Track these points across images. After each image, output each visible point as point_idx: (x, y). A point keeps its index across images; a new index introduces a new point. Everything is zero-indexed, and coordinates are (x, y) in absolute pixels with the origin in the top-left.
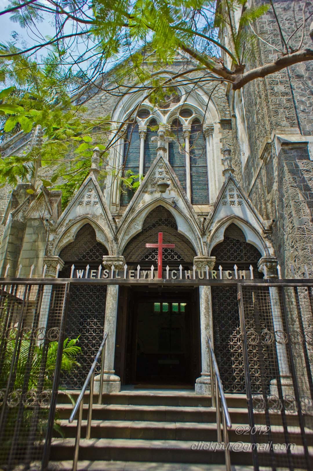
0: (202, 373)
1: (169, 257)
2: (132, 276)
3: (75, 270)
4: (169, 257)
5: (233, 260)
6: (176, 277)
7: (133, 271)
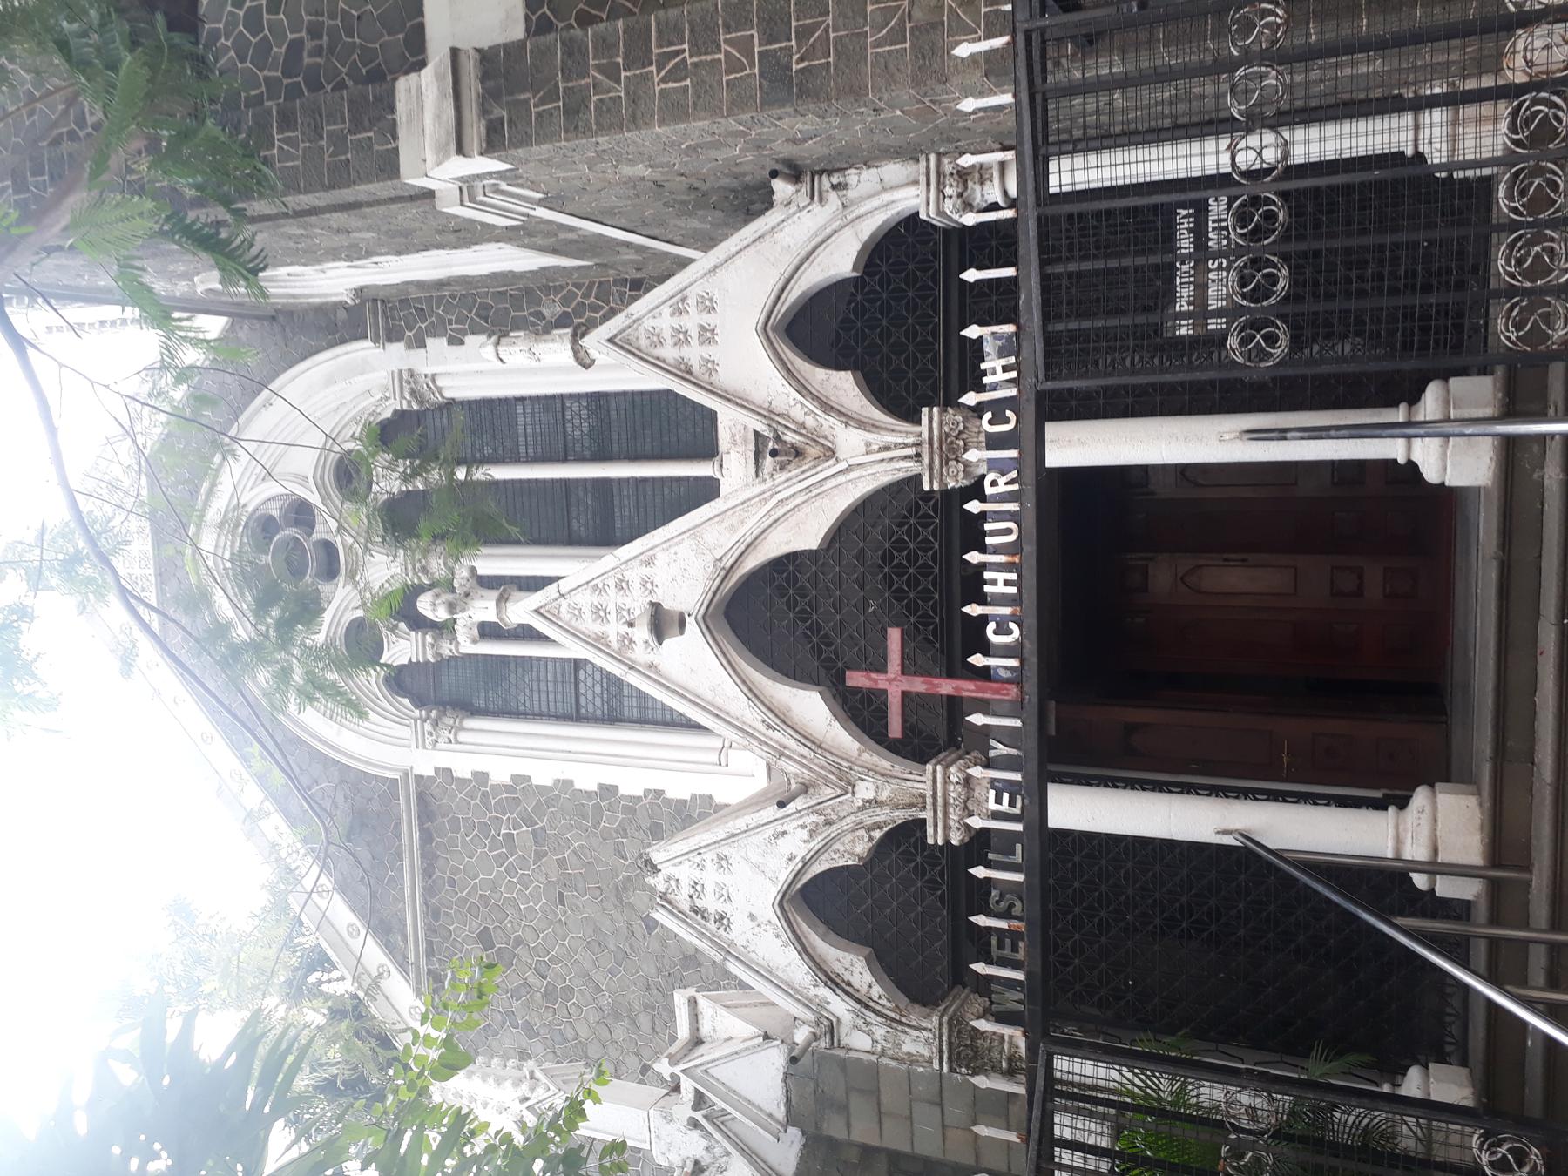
0: (1402, 460)
1: (925, 534)
2: (1015, 949)
4: (925, 534)
5: (936, 301)
6: (1012, 626)
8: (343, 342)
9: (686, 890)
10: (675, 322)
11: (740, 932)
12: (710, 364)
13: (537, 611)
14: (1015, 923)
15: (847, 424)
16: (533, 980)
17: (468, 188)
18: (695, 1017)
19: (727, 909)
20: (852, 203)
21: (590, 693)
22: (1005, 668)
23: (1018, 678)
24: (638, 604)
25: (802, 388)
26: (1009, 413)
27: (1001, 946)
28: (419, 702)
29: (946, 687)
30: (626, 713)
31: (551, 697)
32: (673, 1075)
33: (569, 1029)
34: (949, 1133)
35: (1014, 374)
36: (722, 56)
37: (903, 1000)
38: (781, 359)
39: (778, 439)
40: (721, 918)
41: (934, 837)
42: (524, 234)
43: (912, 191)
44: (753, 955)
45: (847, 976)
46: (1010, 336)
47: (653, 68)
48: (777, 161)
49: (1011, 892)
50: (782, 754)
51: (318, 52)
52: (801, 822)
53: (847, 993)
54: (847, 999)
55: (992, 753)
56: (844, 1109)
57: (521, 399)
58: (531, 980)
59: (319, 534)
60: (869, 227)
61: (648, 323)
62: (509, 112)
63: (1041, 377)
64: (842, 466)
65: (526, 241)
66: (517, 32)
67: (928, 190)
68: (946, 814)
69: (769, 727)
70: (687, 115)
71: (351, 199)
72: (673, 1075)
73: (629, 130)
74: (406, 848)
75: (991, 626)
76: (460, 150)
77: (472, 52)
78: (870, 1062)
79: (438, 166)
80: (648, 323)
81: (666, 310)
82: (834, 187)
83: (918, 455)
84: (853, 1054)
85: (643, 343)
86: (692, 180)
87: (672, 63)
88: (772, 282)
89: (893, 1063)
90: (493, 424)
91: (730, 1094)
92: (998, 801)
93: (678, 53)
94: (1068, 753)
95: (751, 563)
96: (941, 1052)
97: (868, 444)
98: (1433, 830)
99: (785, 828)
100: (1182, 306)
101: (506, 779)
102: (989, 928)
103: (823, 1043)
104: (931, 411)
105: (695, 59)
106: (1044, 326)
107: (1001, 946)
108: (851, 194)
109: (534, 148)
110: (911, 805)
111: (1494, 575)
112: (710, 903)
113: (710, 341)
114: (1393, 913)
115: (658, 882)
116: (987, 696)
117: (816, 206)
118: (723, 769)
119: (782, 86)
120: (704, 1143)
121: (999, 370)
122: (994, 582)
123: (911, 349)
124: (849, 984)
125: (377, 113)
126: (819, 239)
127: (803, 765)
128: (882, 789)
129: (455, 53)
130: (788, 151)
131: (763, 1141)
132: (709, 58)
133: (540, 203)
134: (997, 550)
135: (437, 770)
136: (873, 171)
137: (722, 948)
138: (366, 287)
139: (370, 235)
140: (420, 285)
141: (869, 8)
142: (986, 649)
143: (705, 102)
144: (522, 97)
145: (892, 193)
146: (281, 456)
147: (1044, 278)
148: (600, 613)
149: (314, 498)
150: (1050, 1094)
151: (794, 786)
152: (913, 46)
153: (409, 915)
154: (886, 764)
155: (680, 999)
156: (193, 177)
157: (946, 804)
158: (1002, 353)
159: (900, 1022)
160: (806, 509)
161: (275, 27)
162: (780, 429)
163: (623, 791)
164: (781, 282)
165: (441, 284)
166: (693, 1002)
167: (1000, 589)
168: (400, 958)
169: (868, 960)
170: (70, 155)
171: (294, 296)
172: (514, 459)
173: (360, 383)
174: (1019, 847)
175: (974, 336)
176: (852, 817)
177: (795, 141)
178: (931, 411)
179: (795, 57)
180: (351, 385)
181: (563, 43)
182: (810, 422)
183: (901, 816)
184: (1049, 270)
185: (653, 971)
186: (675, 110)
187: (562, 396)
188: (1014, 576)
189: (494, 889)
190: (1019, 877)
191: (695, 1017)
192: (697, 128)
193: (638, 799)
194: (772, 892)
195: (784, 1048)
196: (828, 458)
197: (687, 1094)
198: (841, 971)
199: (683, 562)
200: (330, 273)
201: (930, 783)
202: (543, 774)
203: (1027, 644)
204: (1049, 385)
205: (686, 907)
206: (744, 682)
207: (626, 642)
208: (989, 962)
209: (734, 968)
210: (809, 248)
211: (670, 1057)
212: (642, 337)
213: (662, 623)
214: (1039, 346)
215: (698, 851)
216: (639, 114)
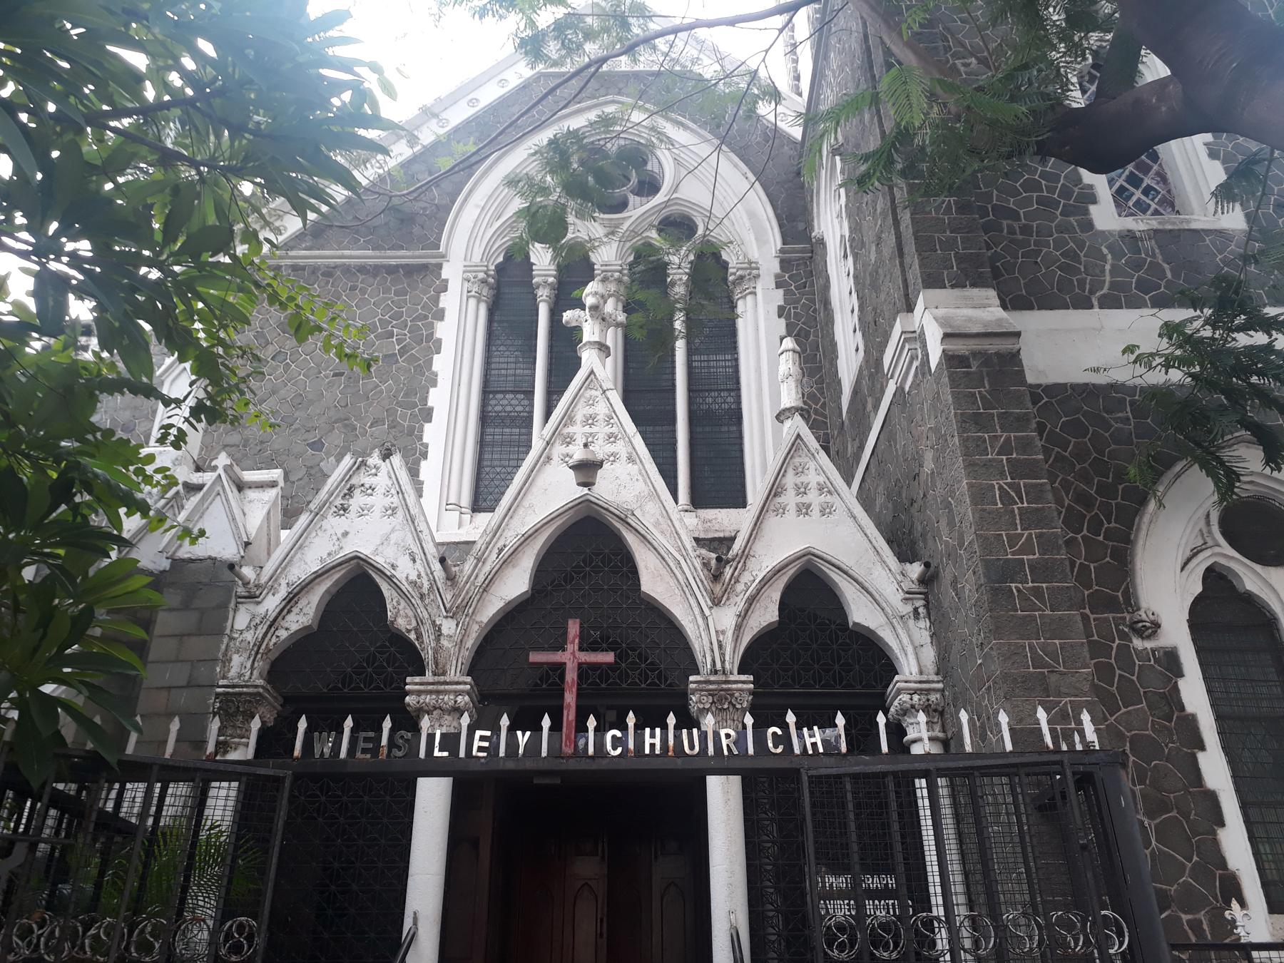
2: (364, 751)
3: (308, 732)
6: (619, 750)
7: (488, 733)
8: (781, 226)
9: (368, 481)
10: (813, 485)
11: (334, 524)
12: (782, 511)
13: (592, 372)
14: (386, 751)
16: (271, 350)
17: (918, 338)
18: (261, 486)
21: (505, 402)
22: (587, 744)
23: (581, 754)
24: (600, 450)
25: (766, 582)
27: (366, 740)
28: (500, 269)
29: (570, 698)
30: (489, 430)
31: (503, 372)
34: (164, 693)
37: (273, 656)
38: (787, 565)
39: (728, 562)
40: (344, 509)
41: (412, 683)
42: (872, 370)
43: (915, 670)
45: (295, 610)
46: (839, 749)
48: (937, 567)
49: (410, 749)
50: (479, 560)
51: (1012, 231)
52: (423, 574)
53: (282, 610)
55: (519, 733)
56: (186, 606)
58: (270, 348)
59: (633, 199)
60: (886, 635)
61: (812, 465)
63: (811, 773)
65: (866, 373)
66: (1031, 379)
68: (431, 692)
69: (501, 551)
70: (976, 505)
71: (906, 250)
74: (383, 253)
75: (619, 734)
76: (946, 336)
77: (1017, 347)
78: (225, 628)
79: (931, 320)
80: (812, 465)
81: (822, 479)
82: (916, 610)
83: (716, 672)
84: (231, 614)
85: (797, 460)
86: (920, 502)
88: (844, 560)
89: (223, 647)
90: (717, 337)
92: (482, 738)
93: (1021, 498)
94: (470, 791)
95: (630, 538)
96: (234, 686)
97: (723, 632)
99: (418, 561)
101: (438, 334)
103: (241, 590)
106: (849, 775)
107: (366, 740)
108: (911, 622)
110: (437, 664)
112: (358, 500)
113: (799, 511)
115: (374, 459)
116: (564, 730)
117: (901, 595)
119: (999, 576)
121: (813, 740)
122: (653, 736)
123: (796, 667)
124: (289, 611)
125: (970, 274)
126: (877, 597)
127: (469, 577)
128: (450, 640)
129: (1017, 335)
130: (947, 574)
133: (900, 389)
134: (678, 738)
135: (447, 281)
137: (321, 509)
138: (825, 247)
139: (873, 257)
140: (827, 286)
141: (1057, 642)
142: (601, 730)
143: (983, 519)
145: (913, 655)
146: (705, 185)
147: (884, 775)
149: (660, 198)
150: (202, 777)
153: (327, 253)
154: (470, 643)
155: (276, 474)
156: (932, 144)
157: (438, 692)
159: (257, 653)
160: (672, 582)
161: (1028, 201)
162: (735, 564)
163: (427, 426)
165: (826, 303)
166: (273, 484)
167: (648, 741)
168: (292, 244)
169: (305, 628)
170: (936, 48)
171: (818, 192)
172: (690, 352)
173: (750, 238)
174: (445, 754)
175: (837, 721)
176: (426, 616)
177: (955, 582)
180: (752, 236)
182: (740, 587)
183: (428, 656)
184: (890, 778)
185: (276, 447)
186: (980, 496)
187: (739, 389)
188: (657, 752)
190: (422, 754)
191: (261, 486)
192: (966, 511)
194: (366, 551)
195: (237, 559)
197: (196, 478)
198: (300, 605)
199: (632, 485)
200: (836, 221)
201: (456, 679)
202: (442, 364)
203: (605, 762)
204: (805, 778)
205: (353, 481)
208: (353, 730)
209: (304, 519)
211: (231, 466)
213: (587, 470)
214: (834, 771)
215: (400, 492)
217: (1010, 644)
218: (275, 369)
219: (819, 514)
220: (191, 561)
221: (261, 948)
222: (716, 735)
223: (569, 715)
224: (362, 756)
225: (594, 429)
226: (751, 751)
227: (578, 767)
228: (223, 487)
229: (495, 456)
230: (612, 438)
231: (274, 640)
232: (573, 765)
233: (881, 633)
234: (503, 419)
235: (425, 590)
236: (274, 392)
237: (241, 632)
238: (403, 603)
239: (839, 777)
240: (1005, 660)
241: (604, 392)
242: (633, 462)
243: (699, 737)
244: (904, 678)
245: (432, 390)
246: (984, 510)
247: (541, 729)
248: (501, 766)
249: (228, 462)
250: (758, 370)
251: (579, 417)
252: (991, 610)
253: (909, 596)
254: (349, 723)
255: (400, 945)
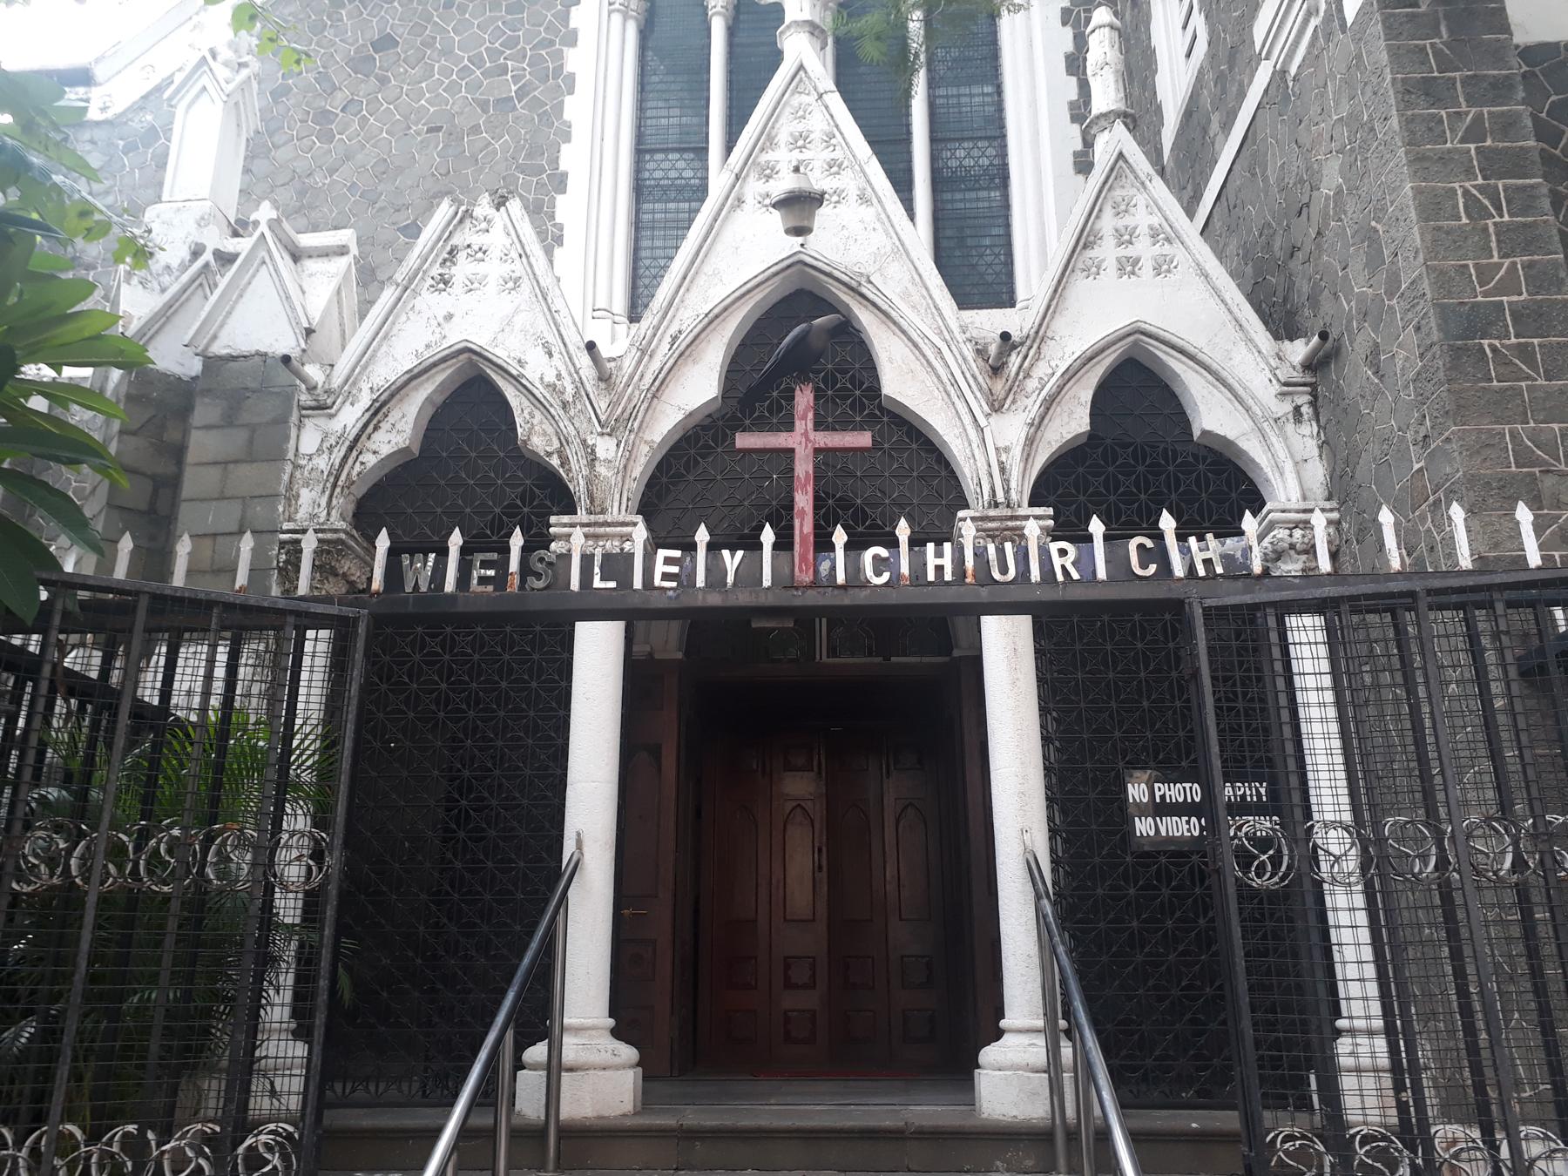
0: (1003, 1023)
3: (393, 553)
6: (886, 576)
7: (677, 553)
9: (478, 241)
10: (1143, 229)
11: (430, 302)
12: (1095, 270)
13: (801, 67)
14: (517, 580)
15: (1032, 425)
16: (340, 97)
18: (325, 253)
19: (458, 286)
20: (1281, 429)
22: (833, 568)
24: (818, 181)
25: (1071, 375)
26: (1153, 568)
29: (803, 500)
30: (646, 206)
32: (256, 223)
33: (284, 138)
35: (1201, 572)
36: (1496, 259)
37: (360, 490)
38: (1102, 350)
40: (445, 281)
43: (1295, 494)
44: (404, 318)
45: (385, 426)
46: (1249, 568)
47: (1480, 181)
49: (555, 576)
50: (643, 352)
52: (564, 374)
53: (365, 426)
54: (359, 425)
55: (726, 553)
56: (229, 421)
57: (999, 91)
58: (339, 95)
60: (1252, 447)
61: (1141, 199)
62: (1424, 14)
63: (1209, 602)
64: (982, 421)
67: (1298, 511)
69: (674, 339)
70: (1427, 220)
72: (256, 223)
73: (1406, 153)
78: (285, 452)
80: (1141, 199)
81: (1156, 220)
82: (1297, 409)
83: (997, 505)
85: (1118, 193)
87: (1486, 202)
89: (286, 477)
91: (237, 291)
92: (668, 561)
93: (1499, 209)
95: (866, 318)
97: (1007, 450)
98: (593, 1069)
99: (556, 355)
100: (1161, 789)
102: (508, 550)
103: (305, 398)
104: (1049, 517)
105: (1491, 229)
108: (1290, 427)
109: (1382, 43)
111: (888, 1123)
112: (463, 268)
113: (1121, 269)
114: (516, 1027)
115: (484, 207)
116: (797, 547)
117: (1277, 388)
118: (589, 313)
119: (1465, 329)
120: (175, 264)
122: (939, 554)
124: (376, 428)
126: (1241, 391)
127: (631, 378)
128: (608, 469)
130: (1356, 349)
131: (187, 326)
132: (1494, 245)
133: (1280, 75)
136: (1316, 452)
137: (411, 281)
141: (1555, 426)
142: (855, 545)
143: (1440, 242)
144: (1443, 30)
148: (801, 141)
151: (609, 365)
152: (1514, 476)
154: (637, 472)
155: (346, 236)
158: (1227, 559)
159: (335, 486)
160: (930, 381)
162: (1024, 350)
164: (1191, 350)
166: (342, 251)
167: (932, 562)
169: (400, 451)
174: (612, 584)
175: (1244, 526)
176: (574, 433)
178: (1049, 517)
179: (1497, 342)
181: (1507, 77)
182: (1032, 384)
183: (578, 487)
186: (1432, 207)
187: (1004, 136)
188: (948, 577)
189: (443, 53)
190: (575, 584)
191: (325, 253)
193: (552, 217)
194: (481, 339)
196: (992, 406)
197: (231, 245)
198: (391, 419)
201: (621, 518)
202: (576, 109)
203: (865, 593)
205: (455, 241)
206: (725, 309)
207: (769, 173)
208: (464, 551)
209: (387, 296)
210: (1231, 381)
211: (278, 221)
212: (1124, 193)
213: (800, 207)
215: (525, 254)
216: (1426, 165)
217: (1480, 431)
218: (347, 126)
219: (1152, 273)
220: (233, 358)
221: (335, 872)
222: (1044, 554)
223: (804, 526)
224: (481, 589)
225: (807, 155)
226: (1102, 573)
227: (822, 601)
228: (269, 251)
229: (658, 243)
230: (834, 166)
231: (358, 468)
232: (812, 598)
233: (1244, 444)
234: (665, 189)
235: (569, 397)
236: (348, 157)
237: (310, 457)
238: (538, 416)
239: (1255, 607)
240: (1471, 456)
241: (820, 96)
242: (868, 202)
243: (1016, 554)
244: (1281, 506)
245: (564, 147)
246: (1439, 229)
247: (760, 546)
248: (699, 601)
249: (274, 214)
250: (1033, 104)
251: (783, 136)
252: (1449, 381)
253: (1288, 388)
254: (456, 540)
255: (558, 874)
